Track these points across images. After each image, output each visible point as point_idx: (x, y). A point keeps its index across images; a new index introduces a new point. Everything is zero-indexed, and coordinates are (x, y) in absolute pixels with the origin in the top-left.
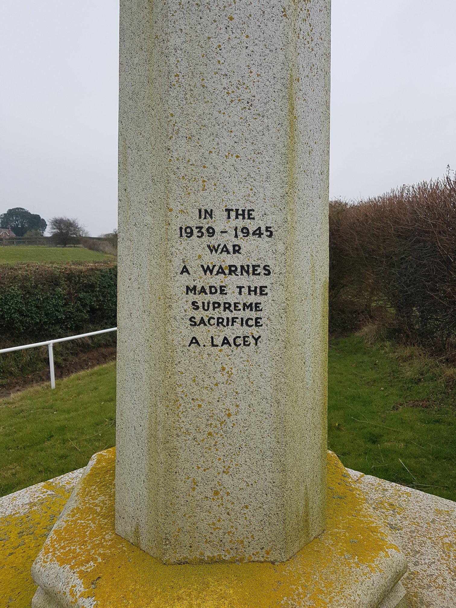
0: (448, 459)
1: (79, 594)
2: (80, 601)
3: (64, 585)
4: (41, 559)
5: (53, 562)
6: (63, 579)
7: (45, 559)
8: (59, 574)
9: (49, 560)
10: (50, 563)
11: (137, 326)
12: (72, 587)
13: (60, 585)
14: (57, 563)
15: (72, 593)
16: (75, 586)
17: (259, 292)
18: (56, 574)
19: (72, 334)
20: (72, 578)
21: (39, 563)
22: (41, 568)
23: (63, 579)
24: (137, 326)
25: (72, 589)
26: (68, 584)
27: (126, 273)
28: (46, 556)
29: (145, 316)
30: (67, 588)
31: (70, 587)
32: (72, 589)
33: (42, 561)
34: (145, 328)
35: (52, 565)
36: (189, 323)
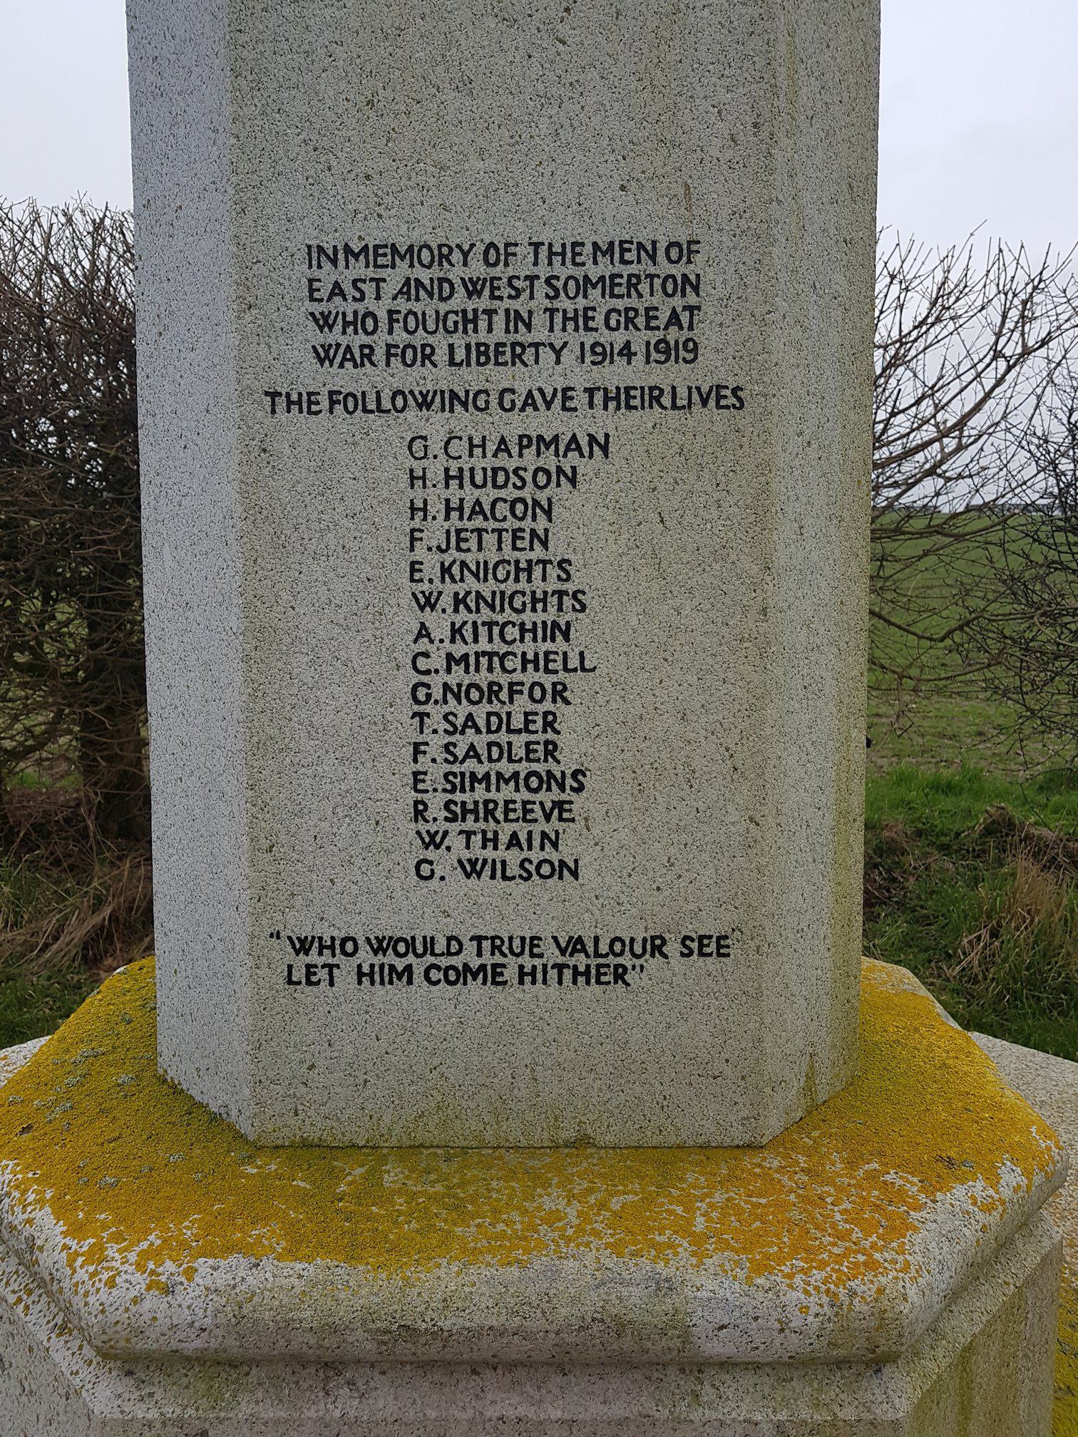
0: (1074, 572)
1: (991, 1192)
2: (1006, 1193)
3: (970, 1224)
4: (896, 1278)
5: (907, 1247)
6: (957, 1223)
7: (898, 1266)
8: (943, 1232)
9: (900, 1258)
10: (910, 1254)
11: (816, 559)
12: (975, 1204)
13: (968, 1233)
14: (908, 1238)
15: (988, 1209)
16: (973, 1198)
17: (465, 473)
18: (943, 1239)
19: (148, 839)
20: (952, 1205)
21: (908, 1285)
22: (920, 1280)
23: (957, 1223)
24: (816, 559)
25: (979, 1204)
26: (968, 1213)
27: (790, 417)
28: (886, 1264)
29: (832, 529)
30: (977, 1218)
31: (976, 1209)
32: (979, 1204)
33: (902, 1274)
34: (831, 561)
35: (917, 1248)
36: (572, 570)
